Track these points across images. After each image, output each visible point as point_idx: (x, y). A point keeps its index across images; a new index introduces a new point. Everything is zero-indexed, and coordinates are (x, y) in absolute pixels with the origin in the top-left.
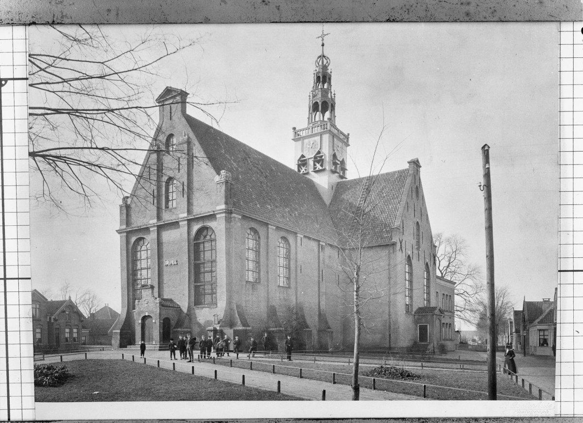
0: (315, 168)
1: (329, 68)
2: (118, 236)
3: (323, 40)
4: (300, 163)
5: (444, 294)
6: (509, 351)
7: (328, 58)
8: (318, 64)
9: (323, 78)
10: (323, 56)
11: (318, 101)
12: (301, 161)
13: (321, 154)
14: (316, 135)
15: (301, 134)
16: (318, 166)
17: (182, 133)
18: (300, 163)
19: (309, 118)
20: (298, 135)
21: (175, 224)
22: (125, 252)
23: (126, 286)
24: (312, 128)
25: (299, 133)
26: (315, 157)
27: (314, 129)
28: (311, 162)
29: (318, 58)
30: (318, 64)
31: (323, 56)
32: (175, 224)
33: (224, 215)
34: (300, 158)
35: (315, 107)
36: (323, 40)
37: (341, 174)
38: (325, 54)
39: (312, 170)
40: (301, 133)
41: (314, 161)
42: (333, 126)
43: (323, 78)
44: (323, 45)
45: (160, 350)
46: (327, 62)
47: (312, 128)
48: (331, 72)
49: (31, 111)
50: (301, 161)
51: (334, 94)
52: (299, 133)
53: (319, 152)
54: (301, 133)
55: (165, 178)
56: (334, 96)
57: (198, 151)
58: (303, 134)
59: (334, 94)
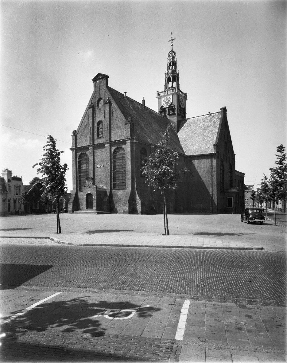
0: (169, 113)
1: (175, 58)
2: (71, 151)
3: (172, 42)
4: (161, 110)
5: (239, 180)
6: (135, 140)
7: (175, 52)
8: (170, 55)
9: (173, 63)
10: (172, 51)
11: (170, 76)
12: (162, 109)
13: (173, 105)
14: (170, 95)
15: (161, 95)
16: (172, 113)
17: (107, 96)
18: (161, 110)
19: (165, 86)
20: (160, 95)
21: (102, 145)
22: (75, 161)
23: (75, 178)
24: (167, 91)
25: (160, 94)
26: (169, 107)
27: (168, 91)
28: (167, 110)
29: (170, 52)
30: (170, 55)
31: (172, 51)
32: (102, 145)
33: (130, 141)
34: (161, 107)
35: (168, 80)
36: (172, 42)
37: (183, 116)
38: (173, 50)
39: (168, 114)
40: (161, 94)
41: (168, 109)
42: (179, 89)
43: (173, 63)
44: (172, 45)
45: (97, 214)
46: (174, 55)
47: (167, 91)
48: (176, 60)
49: (167, 234)
50: (162, 109)
51: (179, 72)
52: (160, 94)
53: (171, 104)
54: (161, 94)
55: (96, 122)
56: (179, 73)
57: (115, 106)
58: (162, 94)
59: (179, 72)
